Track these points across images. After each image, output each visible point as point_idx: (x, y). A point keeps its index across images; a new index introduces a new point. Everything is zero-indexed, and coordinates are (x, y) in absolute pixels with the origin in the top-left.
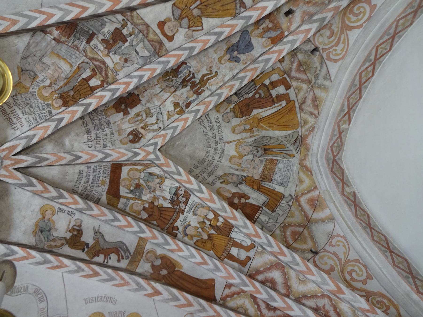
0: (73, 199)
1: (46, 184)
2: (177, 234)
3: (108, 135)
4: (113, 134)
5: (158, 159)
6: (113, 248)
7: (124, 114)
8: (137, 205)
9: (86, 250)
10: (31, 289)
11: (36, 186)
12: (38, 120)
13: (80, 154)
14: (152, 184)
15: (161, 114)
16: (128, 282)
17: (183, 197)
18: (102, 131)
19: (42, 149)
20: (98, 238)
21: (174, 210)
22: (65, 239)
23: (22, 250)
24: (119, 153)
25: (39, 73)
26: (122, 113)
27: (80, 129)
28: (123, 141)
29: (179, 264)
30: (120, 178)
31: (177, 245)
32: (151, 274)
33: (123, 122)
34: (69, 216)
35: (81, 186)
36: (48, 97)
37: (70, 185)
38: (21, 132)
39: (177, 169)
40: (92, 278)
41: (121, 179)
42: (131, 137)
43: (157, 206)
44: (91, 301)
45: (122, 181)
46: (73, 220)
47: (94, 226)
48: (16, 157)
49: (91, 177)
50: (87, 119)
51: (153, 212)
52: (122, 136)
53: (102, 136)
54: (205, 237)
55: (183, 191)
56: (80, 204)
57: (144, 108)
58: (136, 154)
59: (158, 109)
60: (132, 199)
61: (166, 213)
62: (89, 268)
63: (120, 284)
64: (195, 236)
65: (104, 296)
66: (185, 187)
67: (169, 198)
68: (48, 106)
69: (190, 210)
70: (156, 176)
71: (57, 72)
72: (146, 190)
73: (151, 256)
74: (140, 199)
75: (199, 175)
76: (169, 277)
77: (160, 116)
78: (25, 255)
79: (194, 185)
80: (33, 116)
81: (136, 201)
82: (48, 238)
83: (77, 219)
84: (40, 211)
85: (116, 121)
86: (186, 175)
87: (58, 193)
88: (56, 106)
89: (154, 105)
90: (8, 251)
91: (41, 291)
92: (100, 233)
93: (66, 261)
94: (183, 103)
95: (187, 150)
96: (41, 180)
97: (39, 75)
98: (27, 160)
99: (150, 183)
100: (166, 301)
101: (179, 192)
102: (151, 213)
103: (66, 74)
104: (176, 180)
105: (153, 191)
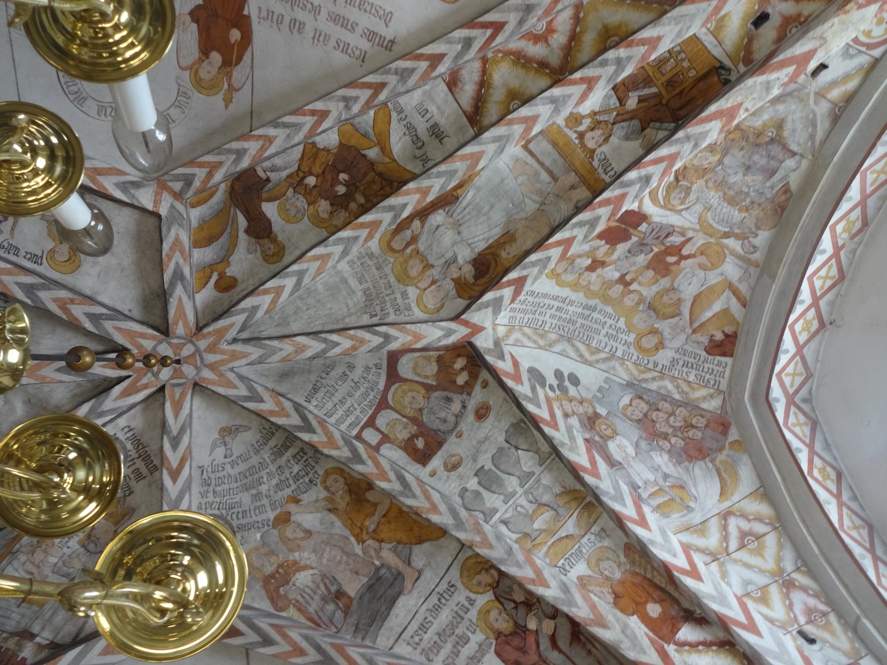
11: (85, 314)
19: (77, 391)
23: (106, 190)
25: (78, 552)
38: (117, 424)
71: (37, 562)
78: (100, 178)
87: (37, 296)
90: (132, 191)
91: (72, 97)
96: (74, 326)
97: (78, 547)
103: (15, 563)
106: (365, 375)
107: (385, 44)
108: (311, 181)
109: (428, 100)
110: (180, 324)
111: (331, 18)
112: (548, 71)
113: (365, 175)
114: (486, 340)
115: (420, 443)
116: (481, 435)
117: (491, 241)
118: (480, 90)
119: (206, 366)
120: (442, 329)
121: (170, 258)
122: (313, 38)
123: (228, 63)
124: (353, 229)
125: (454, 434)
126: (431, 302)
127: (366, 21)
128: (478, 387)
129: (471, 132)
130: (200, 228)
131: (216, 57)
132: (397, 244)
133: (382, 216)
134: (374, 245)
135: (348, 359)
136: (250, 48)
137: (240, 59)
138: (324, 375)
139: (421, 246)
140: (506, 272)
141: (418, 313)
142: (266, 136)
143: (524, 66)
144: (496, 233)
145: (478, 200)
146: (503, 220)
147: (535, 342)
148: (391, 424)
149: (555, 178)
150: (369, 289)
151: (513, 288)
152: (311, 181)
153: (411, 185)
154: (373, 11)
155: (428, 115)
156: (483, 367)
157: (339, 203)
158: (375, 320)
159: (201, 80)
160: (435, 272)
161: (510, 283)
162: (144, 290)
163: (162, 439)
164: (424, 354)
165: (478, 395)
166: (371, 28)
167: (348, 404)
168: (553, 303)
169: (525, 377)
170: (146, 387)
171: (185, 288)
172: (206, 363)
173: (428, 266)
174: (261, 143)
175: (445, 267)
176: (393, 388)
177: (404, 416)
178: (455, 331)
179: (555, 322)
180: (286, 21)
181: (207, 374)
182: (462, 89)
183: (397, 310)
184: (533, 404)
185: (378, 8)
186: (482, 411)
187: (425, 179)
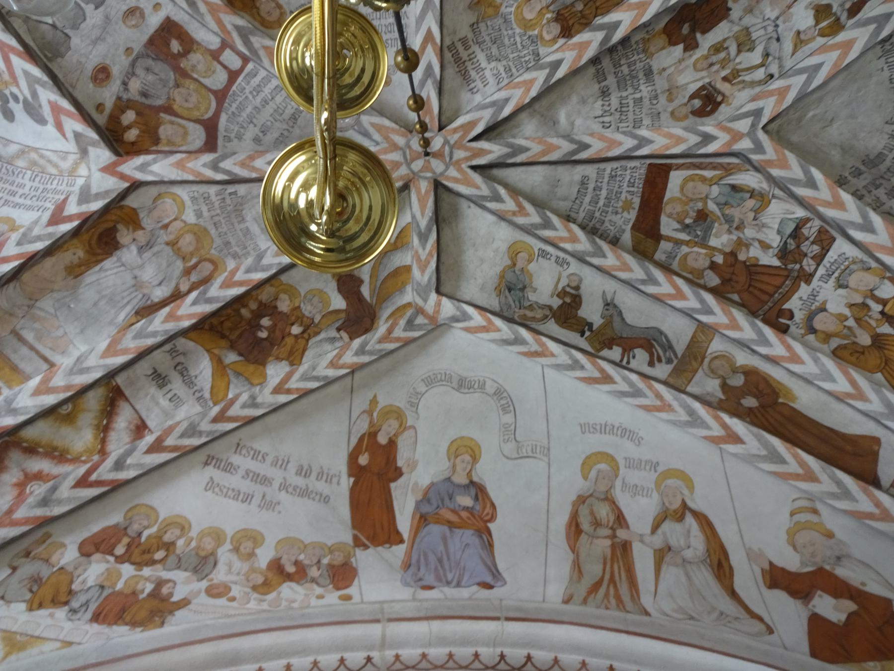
0: (569, 231)
1: (521, 199)
2: (788, 327)
3: (646, 102)
4: (656, 97)
5: (759, 148)
6: (641, 338)
7: (686, 50)
8: (698, 257)
9: (587, 334)
10: (490, 388)
12: (514, 70)
13: (587, 139)
14: (736, 213)
15: (778, 40)
16: (670, 406)
17: (813, 243)
18: (632, 91)
19: (515, 131)
20: (611, 316)
21: (786, 273)
22: (550, 308)
24: (669, 136)
26: (681, 47)
27: (587, 87)
28: (676, 113)
29: (788, 392)
30: (663, 198)
31: (789, 348)
32: (721, 400)
33: (681, 68)
34: (559, 267)
35: (582, 209)
36: (534, 22)
37: (564, 205)
39: (807, 173)
40: (597, 386)
41: (665, 199)
42: (697, 103)
43: (745, 262)
44: (592, 430)
45: (667, 203)
46: (565, 274)
47: (604, 292)
48: (474, 144)
49: (604, 193)
50: (606, 63)
51: (733, 273)
52: (677, 103)
53: (631, 104)
54: (865, 339)
55: (814, 230)
56: (580, 242)
57: (736, 28)
58: (708, 138)
59: (770, 29)
60: (687, 243)
61: (765, 278)
62: (594, 364)
63: (654, 406)
64: (836, 335)
65: (617, 425)
66: (821, 217)
67: (775, 245)
68: (533, 40)
69: (830, 276)
70: (748, 192)
72: (721, 224)
73: (723, 366)
74: (704, 245)
75: (864, 192)
76: (763, 416)
77: (774, 45)
78: (484, 323)
79: (849, 210)
80: (504, 63)
81: (696, 249)
82: (520, 302)
83: (572, 274)
84: (508, 252)
85: (665, 65)
86: (831, 189)
88: (547, 37)
89: (760, 21)
90: (458, 313)
91: (505, 394)
92: (615, 306)
93: (552, 345)
94: (842, 5)
95: (835, 132)
96: (514, 192)
98: (493, 150)
99: (733, 209)
100: (750, 459)
101: (803, 230)
102: (728, 276)
104: (801, 202)
105: (737, 228)
106: (242, 130)
107: (214, 461)
108: (296, 330)
109: (170, 411)
110: (423, 191)
111: (269, 481)
112: (25, 444)
113: (240, 336)
114: (98, 157)
115: (175, 46)
116: (101, 48)
117: (97, 268)
118: (108, 424)
119: (401, 149)
120: (152, 172)
121: (430, 254)
122: (288, 462)
123: (372, 435)
124: (251, 280)
125: (135, 53)
126: (168, 207)
127: (234, 481)
128: (109, 104)
129: (120, 380)
130: (404, 284)
131: (382, 439)
132: (207, 267)
133: (220, 293)
134: (231, 264)
135: (261, 148)
136: (351, 448)
137: (361, 439)
138: (286, 133)
139: (179, 265)
140: (76, 233)
141: (183, 193)
142: (336, 368)
143: (55, 449)
144: (91, 277)
145: (113, 311)
146: (81, 291)
147: (42, 156)
148: (210, 72)
149: (15, 333)
150: (239, 222)
151: (66, 213)
152: (296, 330)
153: (186, 324)
154: (225, 491)
155: (169, 396)
156: (104, 128)
157: (268, 309)
158: (231, 189)
159: (397, 419)
160: (164, 237)
161: (70, 218)
162: (457, 226)
163: (441, 76)
164: (174, 149)
165: (108, 95)
166: (228, 475)
167: (259, 99)
168: (21, 201)
169: (47, 112)
170: (455, 130)
171: (418, 226)
172: (400, 152)
173: (172, 244)
174: (341, 362)
175: (152, 242)
176: (210, 114)
177: (196, 80)
178: (137, 169)
179: (19, 180)
180: (314, 475)
181: (400, 141)
182: (130, 423)
183: (207, 198)
184: (33, 76)
185: (220, 493)
186: (101, 76)
187: (171, 330)
